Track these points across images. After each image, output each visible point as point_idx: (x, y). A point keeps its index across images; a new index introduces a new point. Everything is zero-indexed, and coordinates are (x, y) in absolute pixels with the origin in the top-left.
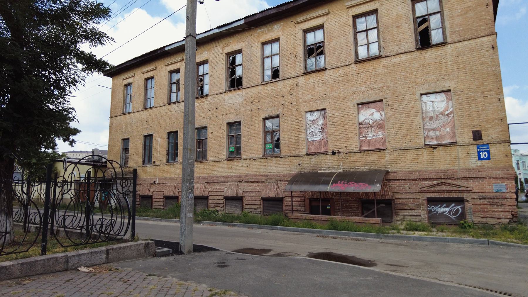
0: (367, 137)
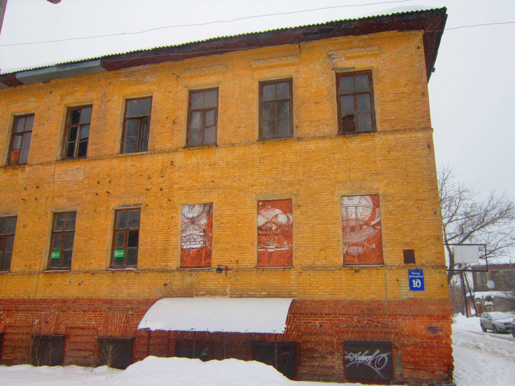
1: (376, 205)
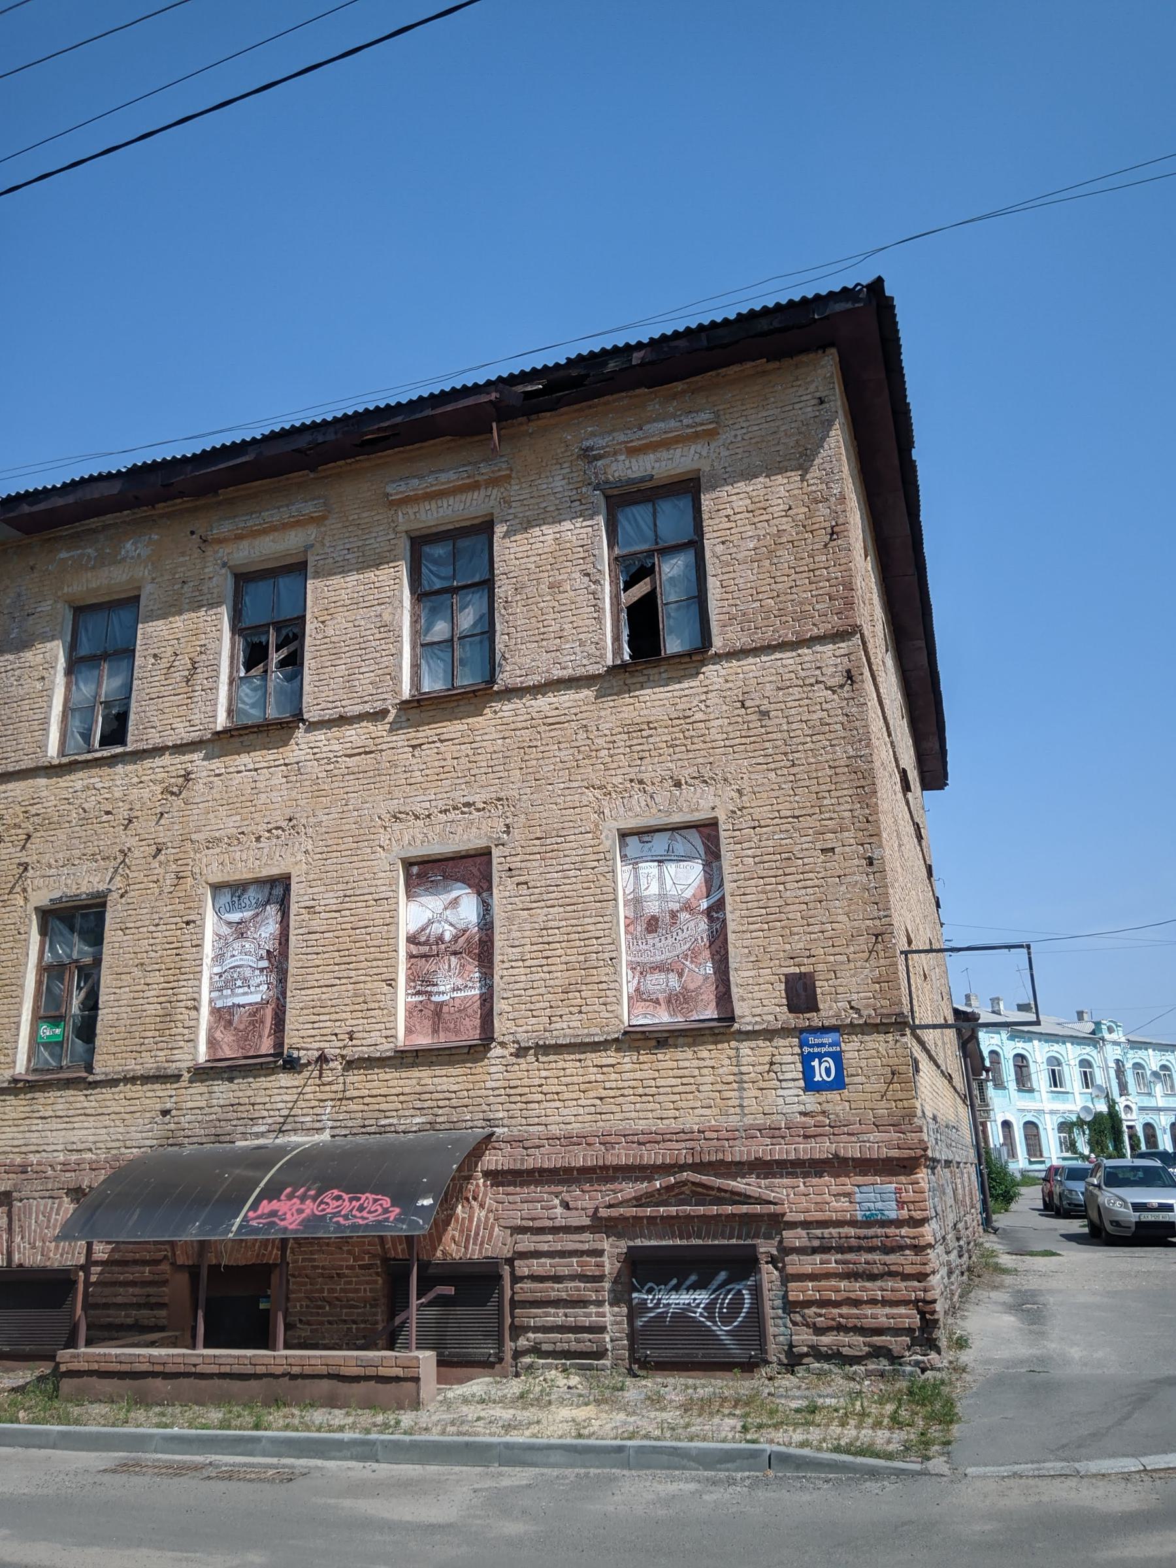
0: (430, 994)
1: (712, 857)
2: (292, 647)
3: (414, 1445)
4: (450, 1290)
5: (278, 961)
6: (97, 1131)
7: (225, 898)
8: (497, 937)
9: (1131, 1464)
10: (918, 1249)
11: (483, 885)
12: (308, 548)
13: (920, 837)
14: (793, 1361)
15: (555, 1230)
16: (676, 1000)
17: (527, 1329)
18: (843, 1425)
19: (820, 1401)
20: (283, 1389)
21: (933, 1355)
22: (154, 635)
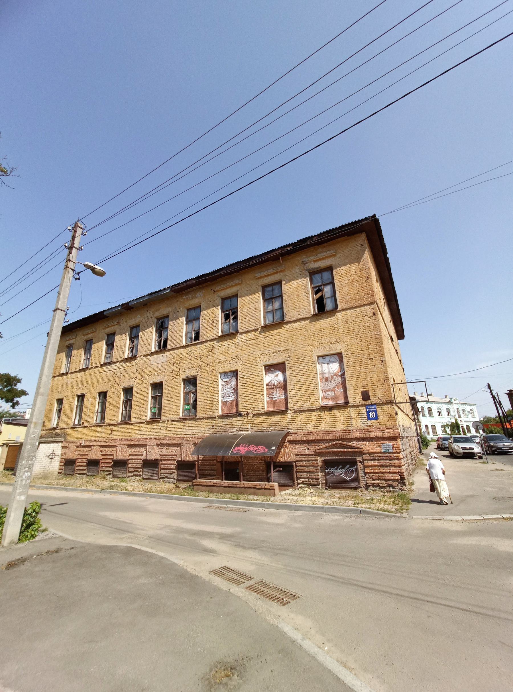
1: (341, 362)
2: (236, 314)
3: (274, 505)
4: (281, 469)
5: (236, 390)
6: (198, 430)
7: (223, 376)
8: (288, 384)
9: (459, 518)
10: (399, 459)
11: (284, 371)
12: (238, 291)
13: (397, 353)
14: (367, 487)
15: (306, 455)
16: (334, 398)
17: (300, 478)
18: (380, 504)
19: (374, 497)
20: (243, 490)
21: (404, 487)
22: (204, 314)
